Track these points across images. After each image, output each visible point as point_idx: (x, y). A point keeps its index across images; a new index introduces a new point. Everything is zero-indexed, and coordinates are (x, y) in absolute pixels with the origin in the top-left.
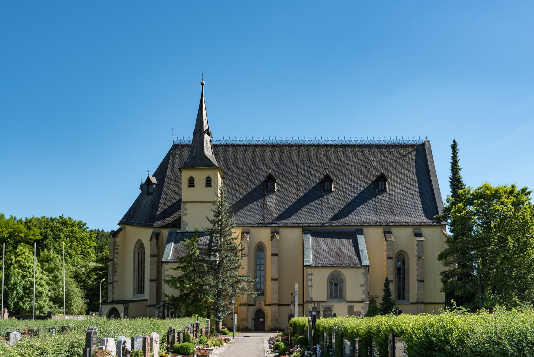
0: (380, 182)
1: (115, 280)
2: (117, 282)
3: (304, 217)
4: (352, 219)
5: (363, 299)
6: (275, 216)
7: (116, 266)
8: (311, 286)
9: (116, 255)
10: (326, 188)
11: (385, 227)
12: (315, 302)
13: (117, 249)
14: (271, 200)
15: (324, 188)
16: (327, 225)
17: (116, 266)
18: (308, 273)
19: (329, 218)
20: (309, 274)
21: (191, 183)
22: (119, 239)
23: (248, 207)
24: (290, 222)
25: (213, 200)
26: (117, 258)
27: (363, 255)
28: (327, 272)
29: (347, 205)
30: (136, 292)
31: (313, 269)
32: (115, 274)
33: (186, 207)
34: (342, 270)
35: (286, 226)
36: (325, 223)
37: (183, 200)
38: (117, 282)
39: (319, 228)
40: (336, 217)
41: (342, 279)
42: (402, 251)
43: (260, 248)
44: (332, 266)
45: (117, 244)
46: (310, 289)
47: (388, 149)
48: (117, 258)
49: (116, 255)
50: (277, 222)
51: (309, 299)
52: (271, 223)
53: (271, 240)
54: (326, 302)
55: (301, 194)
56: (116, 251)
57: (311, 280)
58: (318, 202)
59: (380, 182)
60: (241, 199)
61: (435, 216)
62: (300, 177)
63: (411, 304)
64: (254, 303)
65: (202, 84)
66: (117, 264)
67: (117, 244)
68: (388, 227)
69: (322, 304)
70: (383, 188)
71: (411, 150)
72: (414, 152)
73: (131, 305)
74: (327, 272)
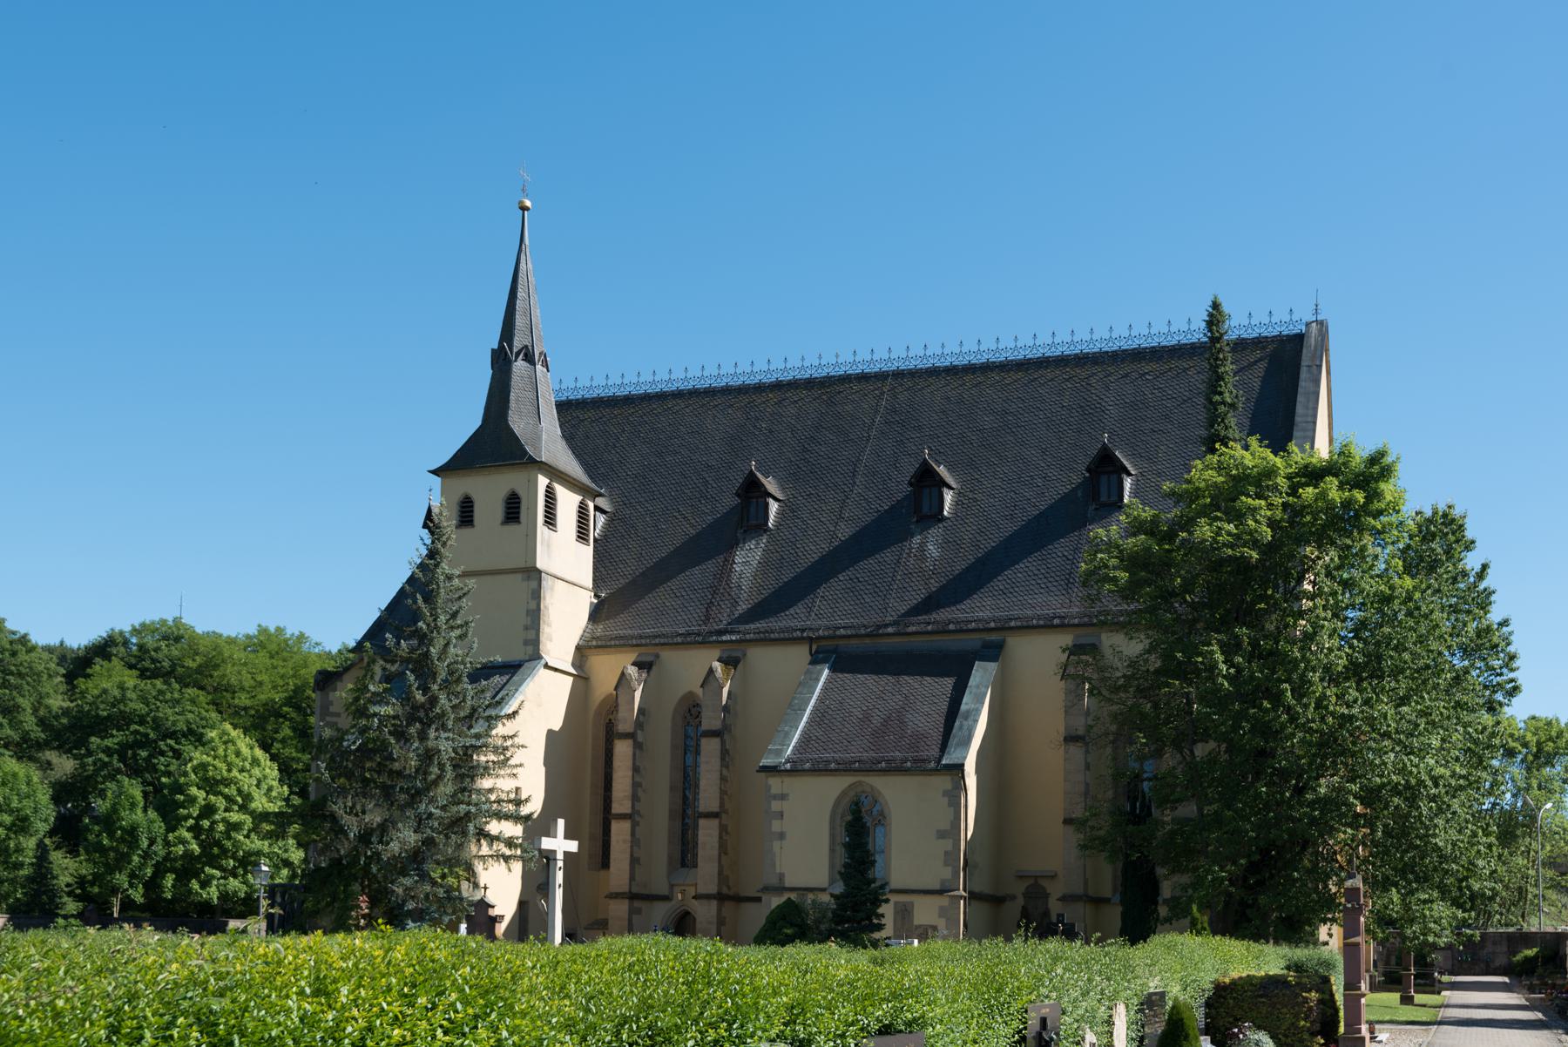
3: (831, 610)
4: (980, 608)
5: (943, 882)
6: (743, 607)
8: (782, 836)
11: (1080, 631)
12: (792, 889)
14: (748, 559)
16: (890, 630)
18: (774, 791)
19: (903, 608)
20: (775, 797)
23: (673, 584)
24: (783, 624)
25: (522, 565)
27: (961, 728)
28: (832, 788)
29: (978, 560)
31: (788, 780)
34: (880, 783)
35: (766, 640)
36: (886, 626)
39: (867, 641)
40: (930, 604)
41: (882, 813)
43: (694, 711)
44: (845, 768)
45: (332, 709)
46: (776, 845)
47: (1173, 364)
50: (742, 628)
51: (774, 881)
52: (721, 632)
55: (845, 532)
57: (781, 815)
58: (888, 556)
60: (662, 560)
61: (566, 559)
62: (859, 479)
64: (665, 891)
65: (524, 208)
67: (332, 709)
68: (1089, 630)
70: (1114, 498)
71: (1258, 354)
72: (1263, 365)
74: (832, 788)
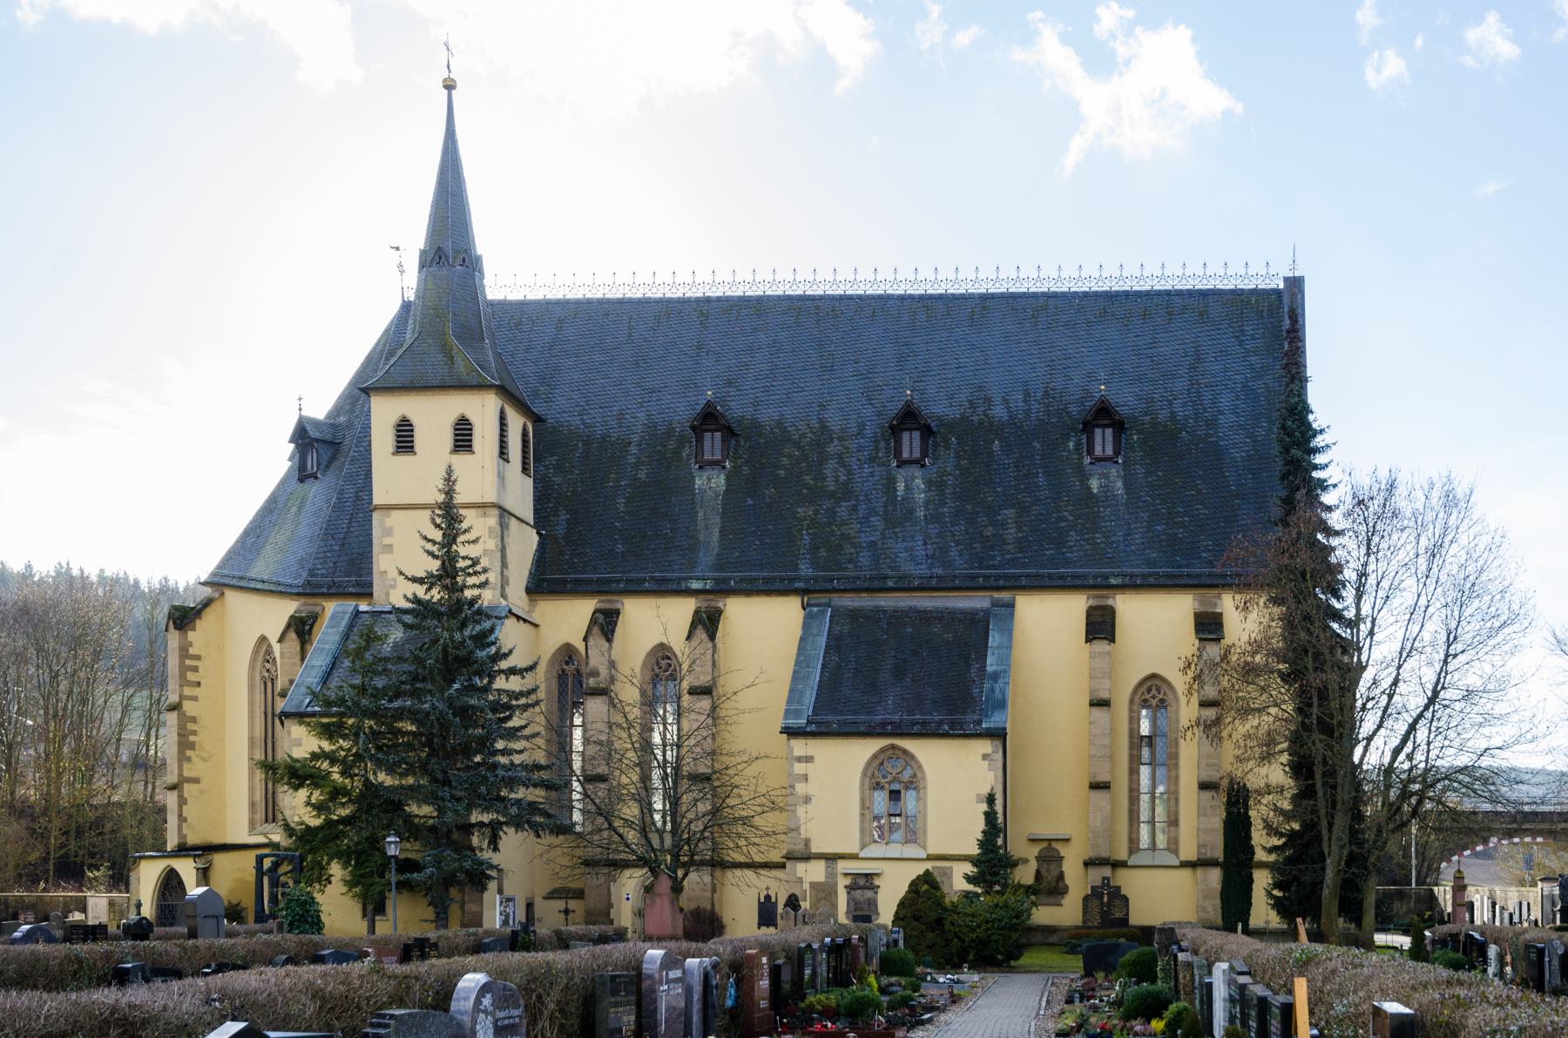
0: (708, 435)
1: (186, 774)
2: (196, 781)
7: (190, 726)
9: (188, 691)
10: (905, 455)
13: (195, 669)
15: (898, 454)
17: (190, 726)
21: (405, 438)
22: (199, 636)
26: (195, 699)
30: (260, 815)
32: (189, 753)
33: (388, 522)
37: (378, 498)
38: (196, 781)
42: (1154, 676)
48: (195, 699)
49: (188, 691)
53: (689, 638)
54: (854, 857)
56: (191, 676)
57: (805, 778)
59: (1098, 432)
63: (1185, 865)
66: (194, 720)
67: (191, 651)
69: (843, 866)
73: (220, 860)
